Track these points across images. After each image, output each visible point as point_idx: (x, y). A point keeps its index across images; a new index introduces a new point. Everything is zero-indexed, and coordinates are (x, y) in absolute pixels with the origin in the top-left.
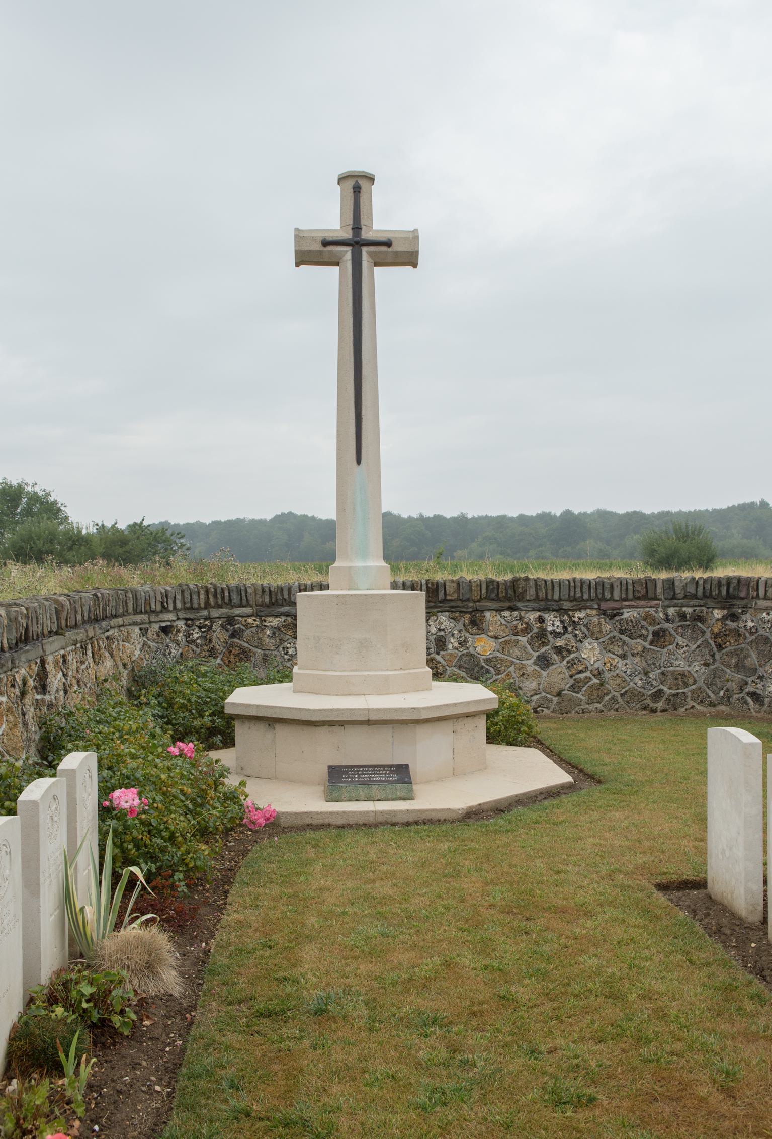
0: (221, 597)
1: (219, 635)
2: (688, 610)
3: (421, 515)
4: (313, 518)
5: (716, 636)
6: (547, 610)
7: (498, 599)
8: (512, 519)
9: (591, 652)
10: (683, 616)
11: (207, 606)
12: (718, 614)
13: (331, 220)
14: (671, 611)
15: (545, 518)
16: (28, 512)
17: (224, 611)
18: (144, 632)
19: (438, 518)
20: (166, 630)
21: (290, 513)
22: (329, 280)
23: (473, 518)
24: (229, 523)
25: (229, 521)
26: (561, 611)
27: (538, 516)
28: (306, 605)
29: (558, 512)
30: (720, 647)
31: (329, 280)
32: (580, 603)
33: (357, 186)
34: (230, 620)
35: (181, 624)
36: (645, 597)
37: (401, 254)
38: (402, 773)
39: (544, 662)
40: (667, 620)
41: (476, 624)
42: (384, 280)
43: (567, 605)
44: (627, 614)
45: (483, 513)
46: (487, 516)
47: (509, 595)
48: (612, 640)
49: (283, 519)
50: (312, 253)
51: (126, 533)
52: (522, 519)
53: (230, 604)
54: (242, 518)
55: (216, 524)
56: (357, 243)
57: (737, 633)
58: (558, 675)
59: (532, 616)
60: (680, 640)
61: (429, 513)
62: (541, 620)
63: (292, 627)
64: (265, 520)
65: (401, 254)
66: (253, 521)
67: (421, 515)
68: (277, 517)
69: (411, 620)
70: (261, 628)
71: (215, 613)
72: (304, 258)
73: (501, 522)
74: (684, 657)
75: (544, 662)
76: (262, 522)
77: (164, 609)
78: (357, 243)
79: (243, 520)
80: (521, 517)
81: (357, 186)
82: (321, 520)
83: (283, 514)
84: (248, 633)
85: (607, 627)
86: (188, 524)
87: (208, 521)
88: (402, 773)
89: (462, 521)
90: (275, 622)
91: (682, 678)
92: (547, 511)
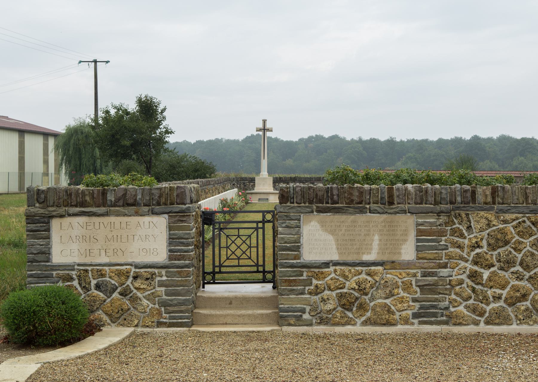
0: (243, 179)
1: (242, 186)
8: (432, 142)
15: (457, 141)
20: (234, 184)
24: (210, 142)
25: (210, 141)
27: (452, 140)
29: (467, 136)
33: (264, 121)
34: (244, 183)
38: (268, 199)
45: (410, 137)
46: (413, 139)
51: (164, 156)
52: (441, 143)
54: (220, 138)
55: (200, 143)
61: (366, 137)
63: (254, 185)
64: (238, 140)
67: (360, 139)
68: (248, 138)
69: (270, 181)
73: (420, 146)
76: (236, 142)
80: (440, 141)
81: (264, 121)
82: (282, 141)
86: (177, 143)
87: (193, 141)
88: (268, 199)
89: (391, 142)
90: (252, 184)
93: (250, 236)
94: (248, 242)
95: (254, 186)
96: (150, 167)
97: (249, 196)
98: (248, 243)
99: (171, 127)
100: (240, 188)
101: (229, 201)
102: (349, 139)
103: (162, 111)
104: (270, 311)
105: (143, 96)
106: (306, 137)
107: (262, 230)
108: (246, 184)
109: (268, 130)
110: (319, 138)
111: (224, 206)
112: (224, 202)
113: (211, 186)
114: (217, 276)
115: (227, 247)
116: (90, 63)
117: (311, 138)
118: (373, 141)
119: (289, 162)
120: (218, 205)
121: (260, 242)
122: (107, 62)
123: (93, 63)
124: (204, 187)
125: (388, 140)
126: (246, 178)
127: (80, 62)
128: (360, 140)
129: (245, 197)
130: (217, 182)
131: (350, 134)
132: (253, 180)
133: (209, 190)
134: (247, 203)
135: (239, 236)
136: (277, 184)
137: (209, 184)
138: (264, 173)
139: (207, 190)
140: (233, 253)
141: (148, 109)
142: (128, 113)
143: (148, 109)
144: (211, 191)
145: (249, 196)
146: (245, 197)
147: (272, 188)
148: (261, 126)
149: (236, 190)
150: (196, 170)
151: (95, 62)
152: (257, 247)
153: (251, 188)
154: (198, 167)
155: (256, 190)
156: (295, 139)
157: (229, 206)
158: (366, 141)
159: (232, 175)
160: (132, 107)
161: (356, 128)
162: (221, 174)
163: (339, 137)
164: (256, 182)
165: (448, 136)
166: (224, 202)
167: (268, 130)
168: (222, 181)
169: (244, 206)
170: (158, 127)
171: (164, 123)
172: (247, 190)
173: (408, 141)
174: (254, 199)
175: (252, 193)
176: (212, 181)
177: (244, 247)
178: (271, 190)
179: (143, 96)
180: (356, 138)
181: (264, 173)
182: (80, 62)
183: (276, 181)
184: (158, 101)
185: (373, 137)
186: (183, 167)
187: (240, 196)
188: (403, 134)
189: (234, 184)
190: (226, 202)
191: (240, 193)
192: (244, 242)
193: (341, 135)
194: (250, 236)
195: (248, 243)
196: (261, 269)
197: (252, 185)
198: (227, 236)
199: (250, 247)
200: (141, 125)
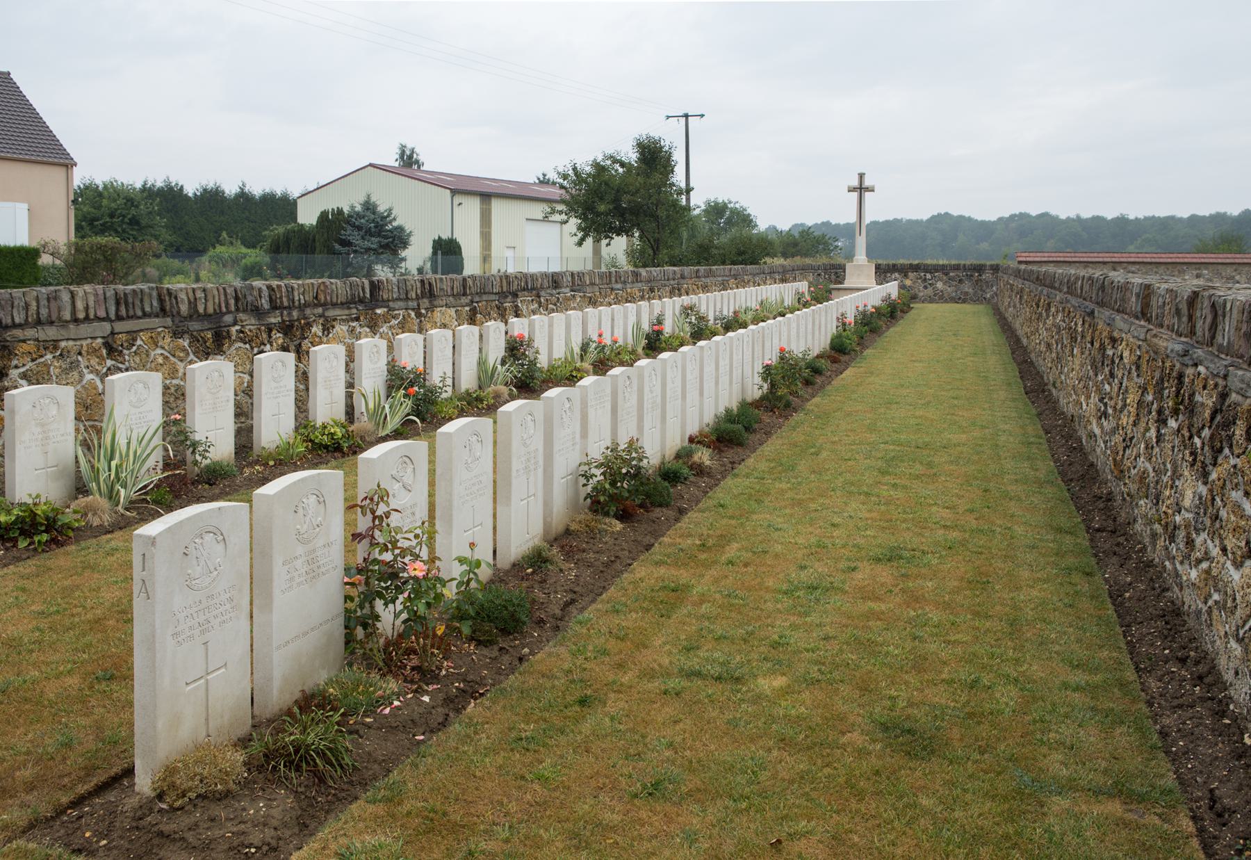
1: (833, 277)
3: (1078, 217)
4: (970, 219)
8: (1181, 220)
9: (940, 285)
15: (1219, 218)
16: (729, 222)
21: (947, 214)
22: (855, 195)
25: (887, 222)
28: (848, 266)
31: (855, 195)
33: (861, 176)
37: (851, 190)
39: (925, 287)
41: (906, 276)
45: (1149, 214)
47: (915, 268)
49: (939, 220)
50: (851, 190)
52: (1194, 220)
56: (861, 188)
58: (930, 291)
61: (1086, 214)
66: (910, 222)
67: (1078, 217)
68: (933, 217)
73: (1167, 224)
74: (967, 287)
75: (925, 287)
76: (918, 223)
78: (861, 188)
81: (861, 176)
83: (939, 215)
89: (1122, 221)
91: (966, 293)
92: (1222, 211)
102: (1063, 216)
104: (275, 692)
106: (1007, 215)
109: (867, 189)
110: (1023, 216)
117: (1013, 217)
118: (1098, 220)
119: (984, 246)
122: (702, 116)
127: (668, 117)
131: (1063, 211)
138: (861, 257)
141: (653, 157)
143: (653, 157)
150: (741, 253)
151: (686, 116)
156: (993, 217)
160: (632, 156)
165: (1205, 211)
167: (867, 189)
173: (1146, 218)
175: (839, 289)
180: (1073, 215)
181: (861, 257)
182: (668, 117)
185: (1096, 214)
188: (1137, 209)
193: (1053, 212)
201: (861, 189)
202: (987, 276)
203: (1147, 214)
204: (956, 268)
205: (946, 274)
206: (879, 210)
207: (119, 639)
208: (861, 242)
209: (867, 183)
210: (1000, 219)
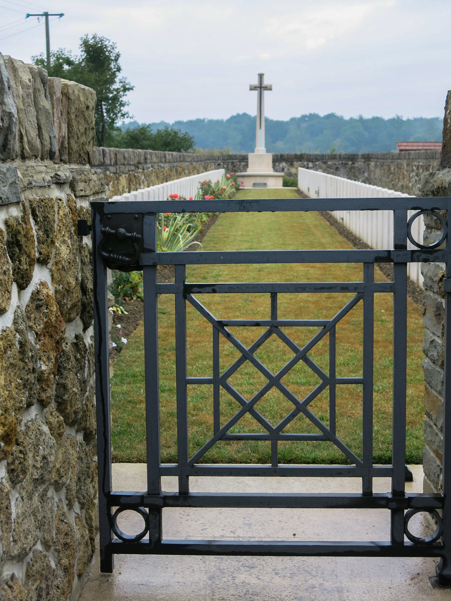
0: (230, 157)
1: (230, 166)
2: (344, 162)
5: (350, 168)
6: (309, 161)
7: (297, 158)
10: (342, 163)
11: (228, 159)
12: (350, 163)
13: (256, 82)
14: (340, 162)
17: (231, 161)
18: (215, 164)
19: (376, 120)
20: (219, 165)
21: (245, 115)
22: (256, 93)
23: (408, 120)
26: (312, 162)
28: (251, 156)
30: (351, 171)
31: (256, 93)
32: (317, 160)
33: (261, 76)
35: (222, 163)
36: (334, 159)
37: (269, 88)
38: (265, 184)
40: (339, 164)
42: (266, 93)
43: (314, 160)
44: (329, 163)
45: (418, 115)
46: (421, 119)
48: (325, 169)
53: (233, 159)
57: (354, 168)
59: (305, 163)
60: (342, 170)
62: (308, 164)
64: (222, 121)
65: (269, 88)
69: (269, 159)
70: (240, 165)
71: (230, 161)
72: (251, 89)
76: (218, 123)
77: (218, 160)
79: (203, 121)
81: (261, 76)
82: (272, 121)
83: (238, 115)
84: (237, 166)
85: (324, 166)
88: (265, 184)
90: (243, 164)
93: (329, 328)
94: (320, 357)
95: (247, 166)
96: (102, 139)
97: (239, 180)
98: (321, 360)
99: (131, 81)
100: (227, 170)
101: (213, 185)
102: (347, 118)
103: (116, 60)
105: (90, 37)
107: (389, 297)
108: (235, 164)
110: (313, 117)
111: (205, 193)
112: (206, 187)
113: (187, 164)
114: (169, 514)
115: (219, 381)
116: (40, 17)
117: (304, 117)
120: (196, 192)
121: (384, 358)
122: (61, 15)
123: (44, 17)
124: (175, 164)
125: (393, 120)
126: (235, 156)
127: (28, 15)
128: (361, 120)
129: (235, 180)
130: (196, 159)
132: (244, 159)
133: (184, 170)
134: (238, 189)
135: (274, 327)
136: (277, 164)
137: (184, 161)
138: (261, 147)
139: (180, 169)
140: (248, 408)
142: (69, 62)
144: (186, 171)
145: (239, 180)
146: (235, 180)
147: (272, 169)
148: (256, 82)
149: (222, 171)
151: (46, 15)
152: (367, 383)
153: (242, 169)
154: (169, 140)
155: (250, 171)
156: (286, 118)
157: (214, 192)
158: (368, 120)
159: (216, 152)
161: (351, 107)
162: (200, 150)
163: (335, 116)
164: (250, 161)
166: (206, 187)
168: (203, 159)
169: (234, 194)
170: (113, 82)
171: (119, 76)
172: (236, 171)
174: (248, 185)
175: (244, 176)
176: (188, 156)
177: (302, 382)
178: (271, 172)
179: (90, 37)
180: (356, 116)
181: (261, 147)
182: (28, 15)
183: (277, 160)
184: (111, 43)
186: (148, 139)
187: (228, 179)
189: (219, 165)
190: (209, 186)
191: (228, 175)
192: (302, 356)
193: (338, 113)
194: (329, 328)
195: (321, 360)
196: (382, 486)
197: (244, 166)
198: (219, 326)
199: (330, 382)
200: (87, 76)
201: (261, 88)
202: (360, 164)
203: (416, 117)
204: (333, 157)
205: (325, 163)
206: (281, 108)
207: (46, 352)
208: (261, 135)
209: (266, 82)
210: (293, 120)
